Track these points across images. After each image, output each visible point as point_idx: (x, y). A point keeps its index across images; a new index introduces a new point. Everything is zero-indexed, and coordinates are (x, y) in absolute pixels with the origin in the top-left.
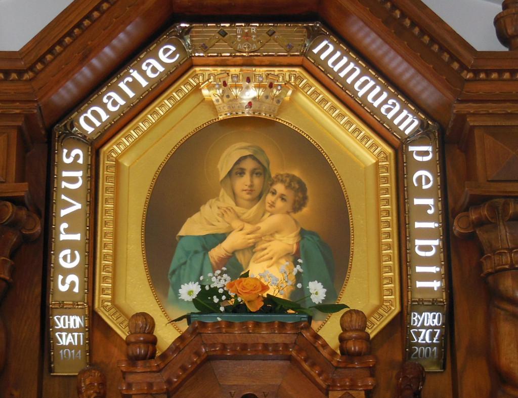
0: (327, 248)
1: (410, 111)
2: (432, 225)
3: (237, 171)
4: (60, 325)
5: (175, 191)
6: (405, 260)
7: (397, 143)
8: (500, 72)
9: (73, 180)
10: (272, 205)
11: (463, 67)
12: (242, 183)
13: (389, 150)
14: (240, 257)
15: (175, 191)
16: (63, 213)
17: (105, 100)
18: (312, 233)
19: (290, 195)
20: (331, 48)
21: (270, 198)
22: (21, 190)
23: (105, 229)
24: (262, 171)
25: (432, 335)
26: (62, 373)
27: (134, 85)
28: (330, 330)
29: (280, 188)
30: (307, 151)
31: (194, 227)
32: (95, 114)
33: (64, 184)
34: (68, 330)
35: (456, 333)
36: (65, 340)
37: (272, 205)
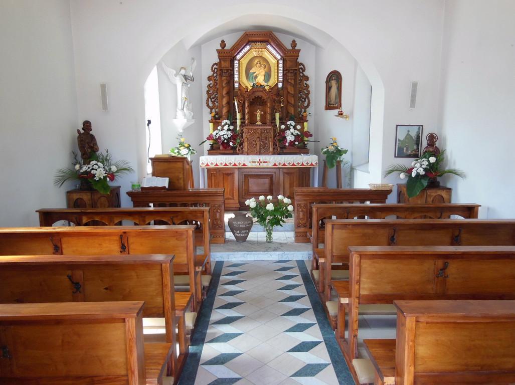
0: (268, 76)
3: (257, 63)
5: (249, 66)
6: (278, 76)
12: (258, 65)
15: (249, 66)
22: (231, 69)
23: (240, 72)
24: (260, 63)
26: (235, 109)
28: (267, 88)
34: (236, 85)
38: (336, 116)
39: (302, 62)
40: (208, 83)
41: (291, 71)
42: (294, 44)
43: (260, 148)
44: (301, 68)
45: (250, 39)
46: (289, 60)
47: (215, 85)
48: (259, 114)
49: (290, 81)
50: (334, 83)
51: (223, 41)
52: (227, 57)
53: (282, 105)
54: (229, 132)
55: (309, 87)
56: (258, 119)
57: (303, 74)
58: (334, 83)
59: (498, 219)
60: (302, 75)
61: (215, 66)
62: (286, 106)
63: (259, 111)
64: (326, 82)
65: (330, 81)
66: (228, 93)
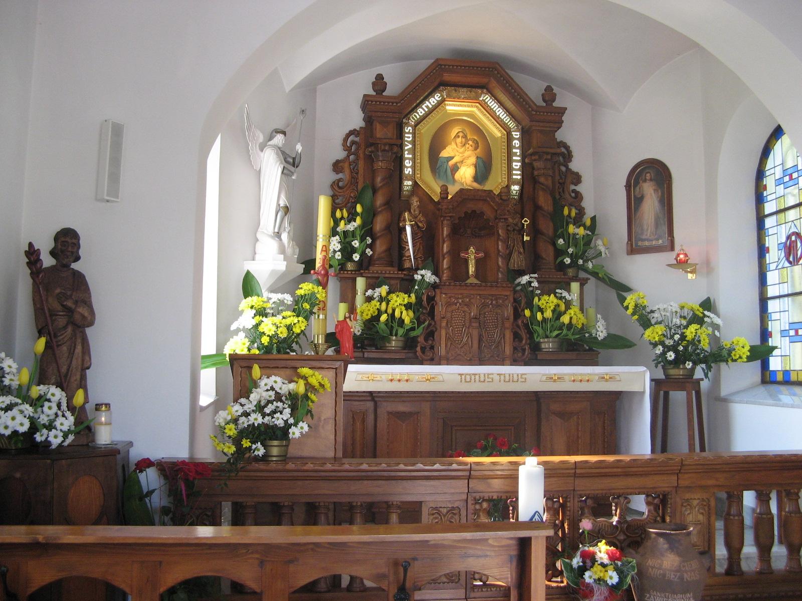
0: (484, 169)
1: (495, 102)
2: (519, 158)
3: (457, 136)
4: (405, 184)
6: (510, 169)
7: (508, 131)
8: (544, 112)
9: (409, 137)
10: (468, 148)
11: (533, 110)
12: (459, 140)
13: (505, 133)
14: (458, 164)
16: (406, 148)
17: (418, 111)
18: (480, 158)
19: (473, 145)
20: (489, 98)
21: (467, 146)
24: (465, 137)
25: (516, 193)
27: (427, 107)
29: (470, 142)
30: (477, 130)
31: (445, 154)
32: (415, 115)
33: (406, 139)
35: (340, 80)
36: (406, 188)
37: (468, 148)
38: (669, 265)
39: (569, 144)
40: (334, 177)
41: (545, 157)
42: (549, 95)
43: (479, 347)
44: (563, 154)
45: (447, 77)
46: (541, 131)
47: (354, 180)
48: (472, 256)
49: (542, 180)
50: (649, 190)
51: (380, 77)
52: (391, 115)
53: (526, 238)
54: (285, 330)
55: (582, 198)
56: (472, 269)
57: (567, 167)
58: (649, 190)
59: (140, 538)
60: (563, 169)
61: (352, 138)
62: (534, 240)
63: (472, 249)
64: (628, 186)
65: (637, 183)
66: (388, 204)
